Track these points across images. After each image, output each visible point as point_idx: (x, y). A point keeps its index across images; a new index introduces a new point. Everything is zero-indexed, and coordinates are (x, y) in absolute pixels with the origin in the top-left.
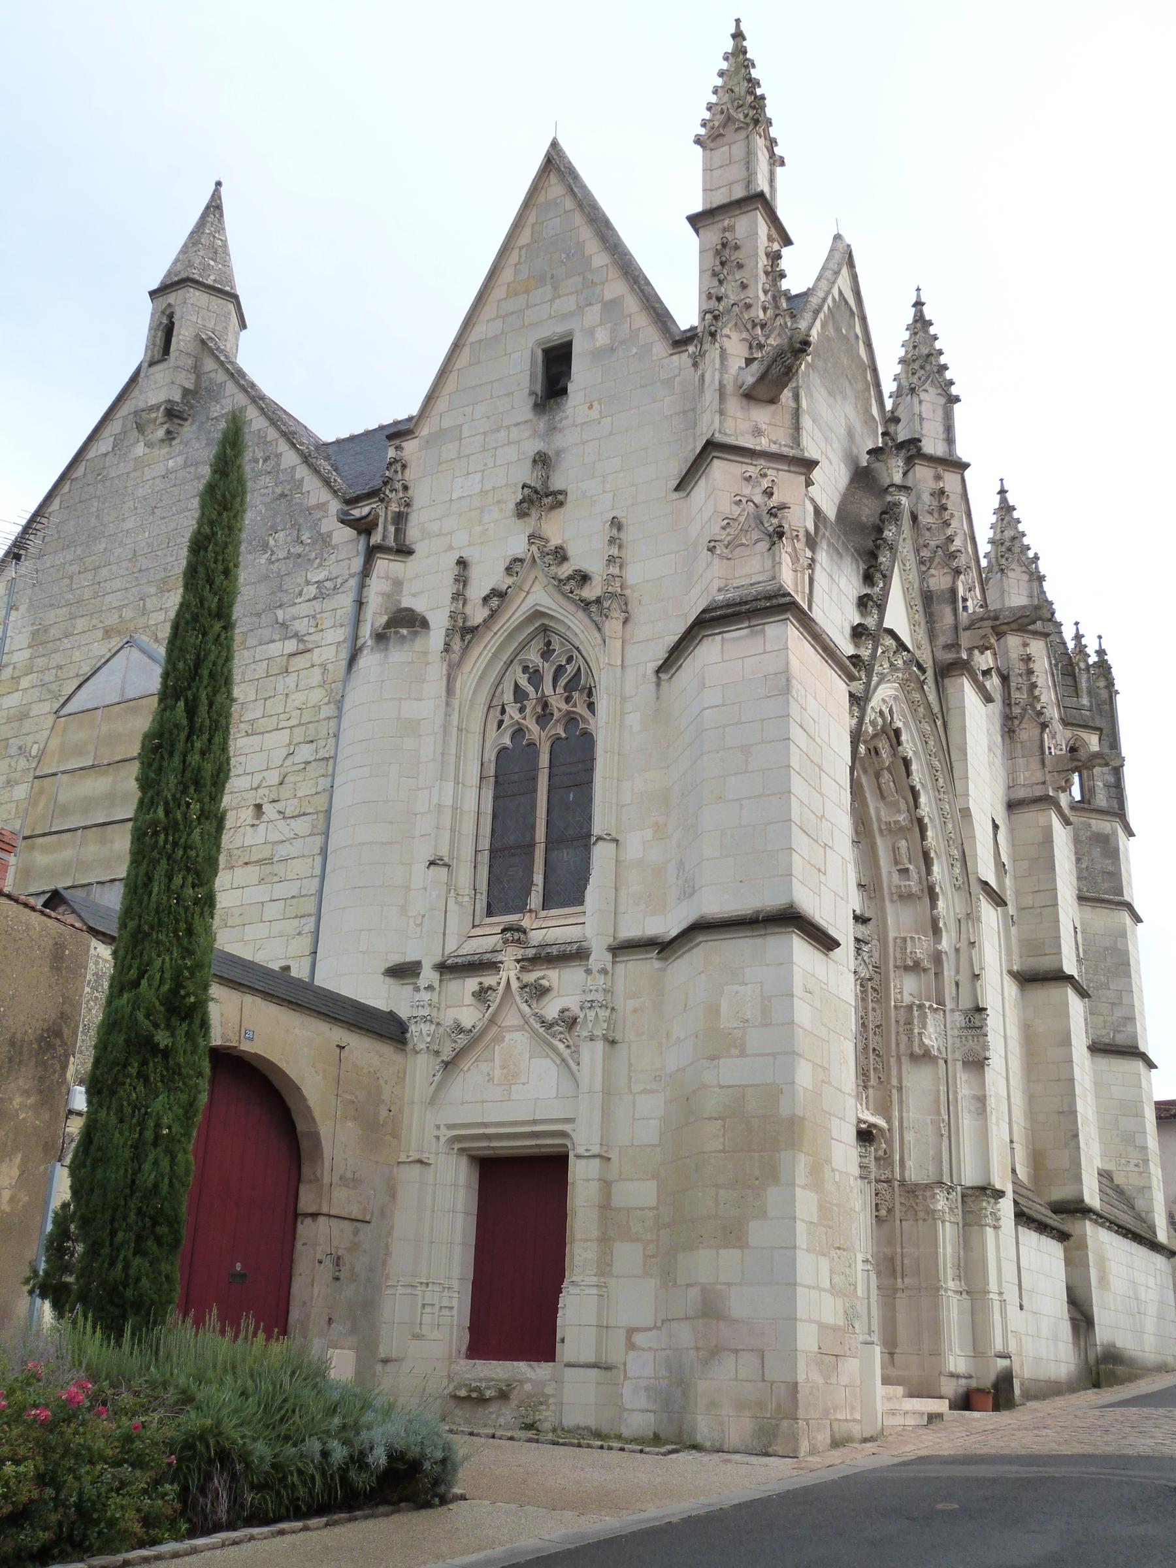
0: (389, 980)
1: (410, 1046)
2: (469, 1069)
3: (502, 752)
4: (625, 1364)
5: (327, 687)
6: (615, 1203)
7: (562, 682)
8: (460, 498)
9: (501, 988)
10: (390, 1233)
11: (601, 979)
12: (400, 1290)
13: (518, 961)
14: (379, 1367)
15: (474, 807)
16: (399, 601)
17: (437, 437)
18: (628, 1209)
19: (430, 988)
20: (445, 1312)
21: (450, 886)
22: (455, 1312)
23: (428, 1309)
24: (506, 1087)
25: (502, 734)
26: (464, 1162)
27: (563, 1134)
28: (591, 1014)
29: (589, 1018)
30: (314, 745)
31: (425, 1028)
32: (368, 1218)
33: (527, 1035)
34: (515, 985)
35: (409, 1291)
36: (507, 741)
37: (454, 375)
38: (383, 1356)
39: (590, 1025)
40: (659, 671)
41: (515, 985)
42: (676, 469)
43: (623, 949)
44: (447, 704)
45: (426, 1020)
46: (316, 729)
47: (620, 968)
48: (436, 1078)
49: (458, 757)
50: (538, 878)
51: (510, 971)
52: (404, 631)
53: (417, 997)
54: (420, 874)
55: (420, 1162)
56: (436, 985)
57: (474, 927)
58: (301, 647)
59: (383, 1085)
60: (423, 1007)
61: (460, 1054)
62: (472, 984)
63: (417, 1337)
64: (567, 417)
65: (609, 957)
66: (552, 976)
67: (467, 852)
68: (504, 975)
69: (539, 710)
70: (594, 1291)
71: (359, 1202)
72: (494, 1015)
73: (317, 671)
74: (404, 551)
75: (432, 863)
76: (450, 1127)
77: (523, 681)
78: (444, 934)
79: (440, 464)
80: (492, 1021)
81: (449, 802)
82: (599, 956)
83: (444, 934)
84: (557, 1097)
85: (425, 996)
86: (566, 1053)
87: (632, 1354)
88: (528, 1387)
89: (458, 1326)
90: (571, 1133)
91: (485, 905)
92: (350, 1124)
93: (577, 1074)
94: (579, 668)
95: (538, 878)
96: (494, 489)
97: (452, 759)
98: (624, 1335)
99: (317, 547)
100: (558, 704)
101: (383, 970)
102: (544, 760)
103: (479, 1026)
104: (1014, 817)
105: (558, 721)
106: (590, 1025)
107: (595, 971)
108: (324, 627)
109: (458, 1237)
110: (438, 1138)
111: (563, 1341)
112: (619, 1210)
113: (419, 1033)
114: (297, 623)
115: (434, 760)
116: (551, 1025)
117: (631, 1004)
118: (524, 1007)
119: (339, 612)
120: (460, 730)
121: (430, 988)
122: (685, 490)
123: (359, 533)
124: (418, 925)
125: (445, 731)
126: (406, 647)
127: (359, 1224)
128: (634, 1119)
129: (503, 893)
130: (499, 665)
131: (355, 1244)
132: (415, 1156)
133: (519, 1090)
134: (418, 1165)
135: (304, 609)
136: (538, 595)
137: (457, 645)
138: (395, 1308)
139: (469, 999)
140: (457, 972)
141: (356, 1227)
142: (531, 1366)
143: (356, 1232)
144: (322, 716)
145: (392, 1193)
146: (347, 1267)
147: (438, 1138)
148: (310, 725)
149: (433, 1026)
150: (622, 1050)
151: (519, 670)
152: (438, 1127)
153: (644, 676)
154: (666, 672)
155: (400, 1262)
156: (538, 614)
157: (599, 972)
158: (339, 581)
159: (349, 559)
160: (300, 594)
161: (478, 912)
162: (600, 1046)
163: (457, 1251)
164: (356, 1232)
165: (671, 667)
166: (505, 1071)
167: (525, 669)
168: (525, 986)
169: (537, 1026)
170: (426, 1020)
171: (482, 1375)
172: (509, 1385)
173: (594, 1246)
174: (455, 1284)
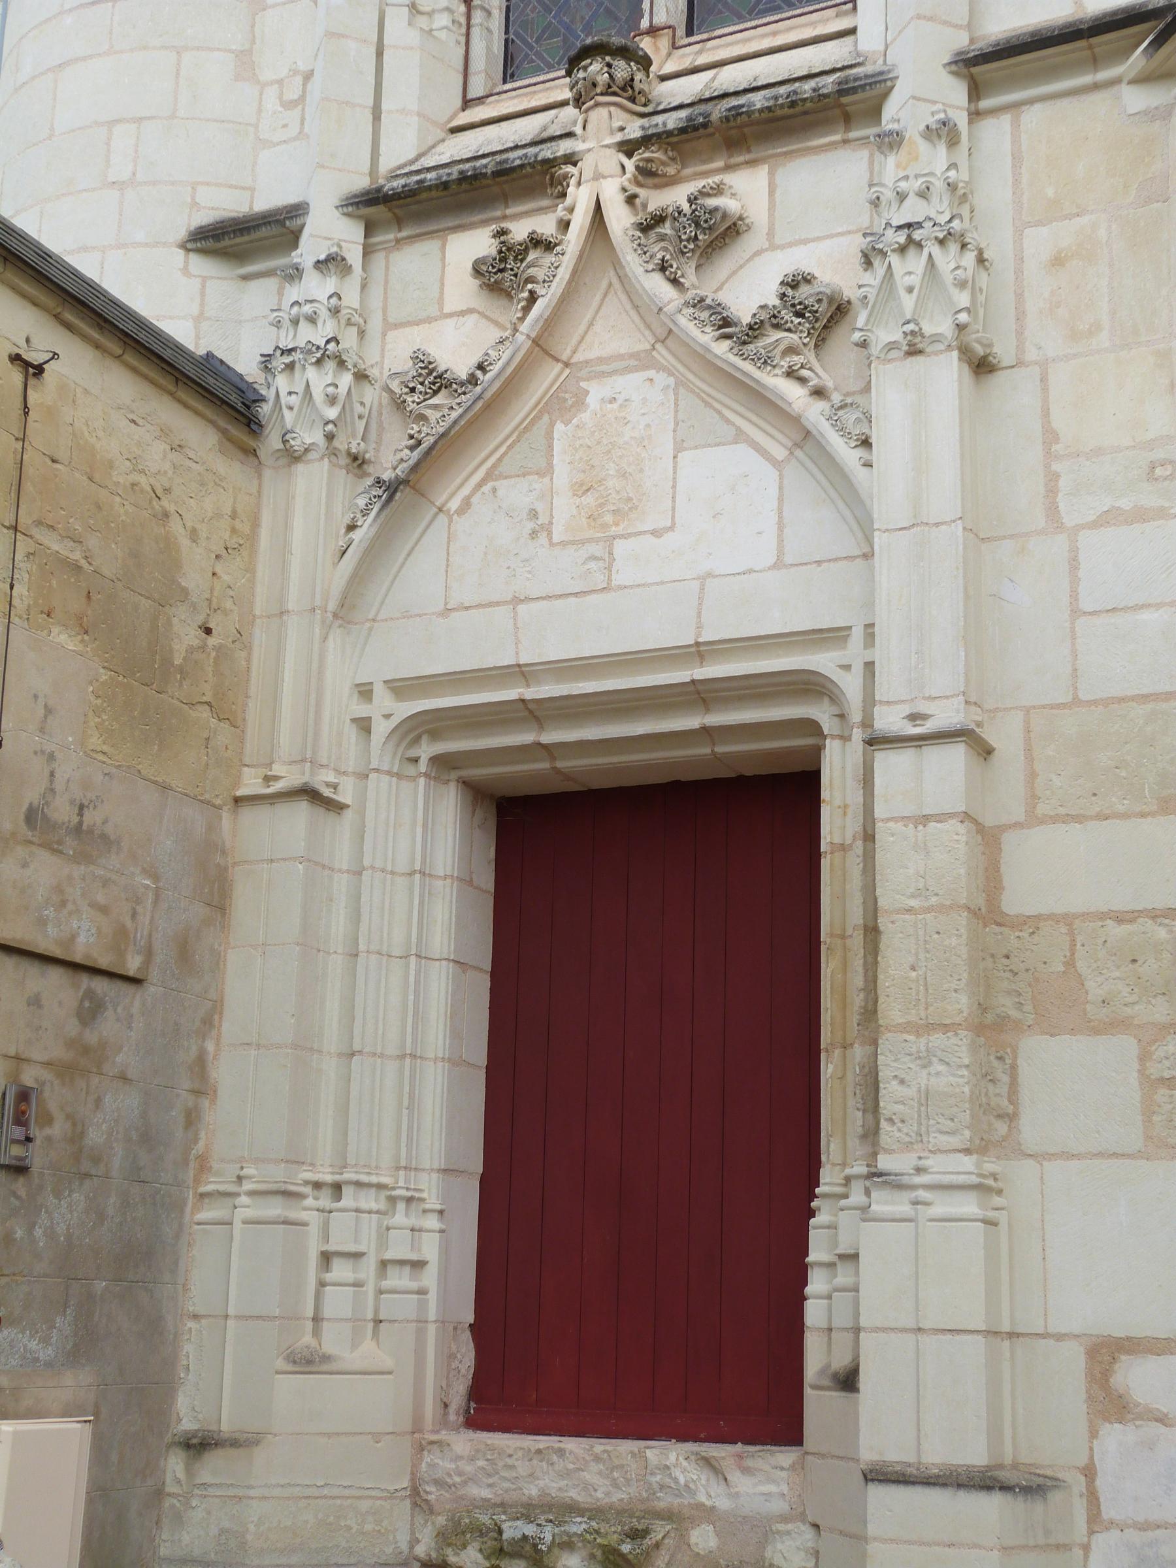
0: (200, 265)
1: (272, 441)
2: (466, 504)
4: (1089, 1472)
6: (1014, 903)
10: (209, 1023)
11: (936, 159)
12: (247, 1208)
13: (628, 148)
14: (175, 1464)
18: (1068, 919)
19: (332, 263)
20: (398, 1279)
22: (430, 1278)
23: (341, 1271)
24: (597, 549)
26: (449, 806)
27: (810, 685)
31: (319, 380)
32: (132, 966)
33: (661, 379)
34: (620, 220)
35: (275, 1209)
38: (188, 1424)
39: (908, 303)
41: (620, 220)
45: (328, 356)
47: (996, 133)
48: (357, 535)
51: (601, 179)
53: (294, 292)
55: (309, 794)
56: (354, 256)
57: (467, 103)
59: (185, 542)
60: (312, 319)
61: (433, 458)
62: (475, 243)
63: (308, 1362)
65: (956, 93)
66: (746, 189)
68: (580, 198)
70: (969, 1206)
71: (104, 910)
72: (550, 324)
76: (401, 688)
80: (541, 346)
82: (923, 89)
84: (778, 565)
86: (815, 413)
87: (1115, 1439)
88: (703, 1538)
89: (441, 1322)
90: (836, 676)
91: (498, 49)
92: (64, 639)
93: (860, 474)
98: (1081, 1362)
101: (182, 234)
104: (815, 769)
107: (913, 133)
109: (436, 1037)
110: (364, 725)
111: (848, 1381)
112: (1033, 923)
113: (299, 403)
116: (755, 330)
117: (1041, 242)
118: (658, 286)
121: (332, 263)
124: (289, 105)
127: (100, 985)
128: (1076, 612)
131: (86, 1050)
132: (291, 778)
133: (638, 546)
134: (303, 808)
138: (231, 1272)
139: (462, 287)
140: (420, 217)
141: (90, 994)
142: (708, 1462)
143: (91, 1011)
145: (216, 893)
146: (58, 1129)
147: (364, 725)
150: (1014, 392)
152: (365, 692)
155: (244, 1115)
157: (929, 133)
161: (478, 62)
162: (946, 372)
163: (434, 1084)
164: (91, 1011)
166: (590, 500)
169: (706, 337)
170: (328, 356)
171: (532, 1491)
172: (636, 1535)
173: (959, 1047)
174: (430, 1188)
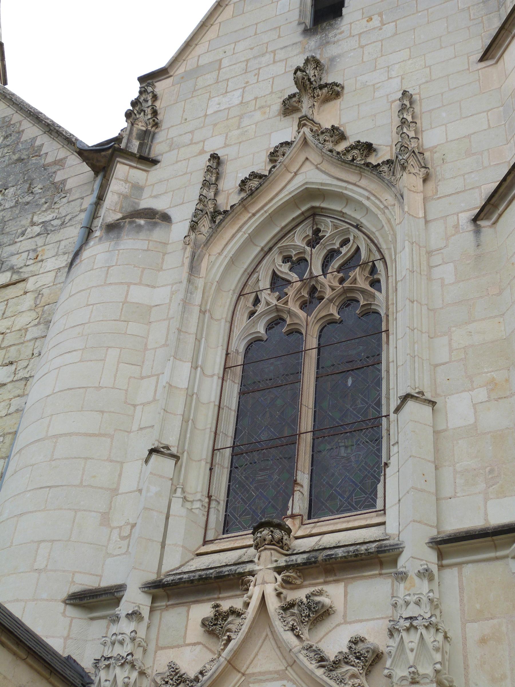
0: (71, 611)
3: (254, 344)
5: (39, 310)
7: (336, 263)
8: (216, 112)
9: (251, 611)
11: (424, 586)
13: (279, 570)
15: (214, 397)
16: (138, 204)
17: (197, 71)
19: (134, 615)
21: (176, 486)
25: (255, 323)
28: (411, 640)
29: (408, 646)
30: (13, 367)
34: (273, 604)
36: (261, 329)
37: (215, 27)
39: (411, 656)
40: (475, 220)
41: (273, 604)
42: (479, 46)
43: (450, 545)
44: (189, 281)
46: (19, 351)
47: (451, 576)
49: (198, 340)
50: (303, 477)
51: (265, 585)
52: (142, 222)
53: (114, 629)
54: (133, 472)
56: (145, 612)
58: (15, 277)
60: (121, 643)
62: (203, 610)
64: (342, 32)
65: (432, 556)
66: (333, 593)
67: (201, 447)
68: (255, 592)
69: (305, 293)
72: (237, 653)
73: (30, 297)
74: (147, 161)
75: (153, 451)
77: (284, 269)
78: (163, 545)
79: (195, 90)
80: (232, 664)
81: (184, 385)
83: (163, 545)
85: (126, 627)
91: (222, 518)
94: (358, 249)
95: (303, 477)
96: (256, 98)
97: (191, 339)
99: (49, 193)
100: (329, 283)
101: (65, 596)
102: (312, 341)
103: (212, 670)
105: (331, 301)
106: (411, 656)
108: (44, 258)
114: (12, 258)
115: (166, 345)
116: (336, 664)
117: (475, 631)
118: (289, 637)
119: (63, 243)
120: (203, 312)
122: (493, 58)
123: (96, 174)
124: (123, 538)
125: (184, 307)
126: (142, 235)
129: (252, 496)
130: (254, 251)
135: (26, 245)
136: (311, 173)
137: (205, 225)
139: (195, 632)
144: (29, 336)
148: (12, 348)
149: (135, 675)
151: (279, 260)
153: (456, 226)
154: (487, 217)
156: (310, 193)
157: (419, 574)
158: (68, 218)
159: (82, 198)
160: (23, 234)
161: (212, 524)
165: (492, 213)
167: (287, 259)
168: (292, 605)
169: (312, 666)
